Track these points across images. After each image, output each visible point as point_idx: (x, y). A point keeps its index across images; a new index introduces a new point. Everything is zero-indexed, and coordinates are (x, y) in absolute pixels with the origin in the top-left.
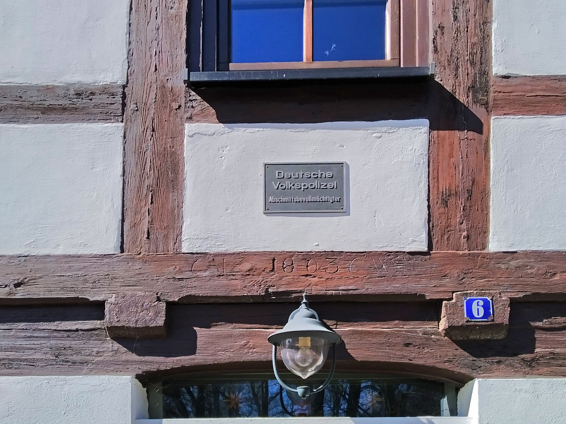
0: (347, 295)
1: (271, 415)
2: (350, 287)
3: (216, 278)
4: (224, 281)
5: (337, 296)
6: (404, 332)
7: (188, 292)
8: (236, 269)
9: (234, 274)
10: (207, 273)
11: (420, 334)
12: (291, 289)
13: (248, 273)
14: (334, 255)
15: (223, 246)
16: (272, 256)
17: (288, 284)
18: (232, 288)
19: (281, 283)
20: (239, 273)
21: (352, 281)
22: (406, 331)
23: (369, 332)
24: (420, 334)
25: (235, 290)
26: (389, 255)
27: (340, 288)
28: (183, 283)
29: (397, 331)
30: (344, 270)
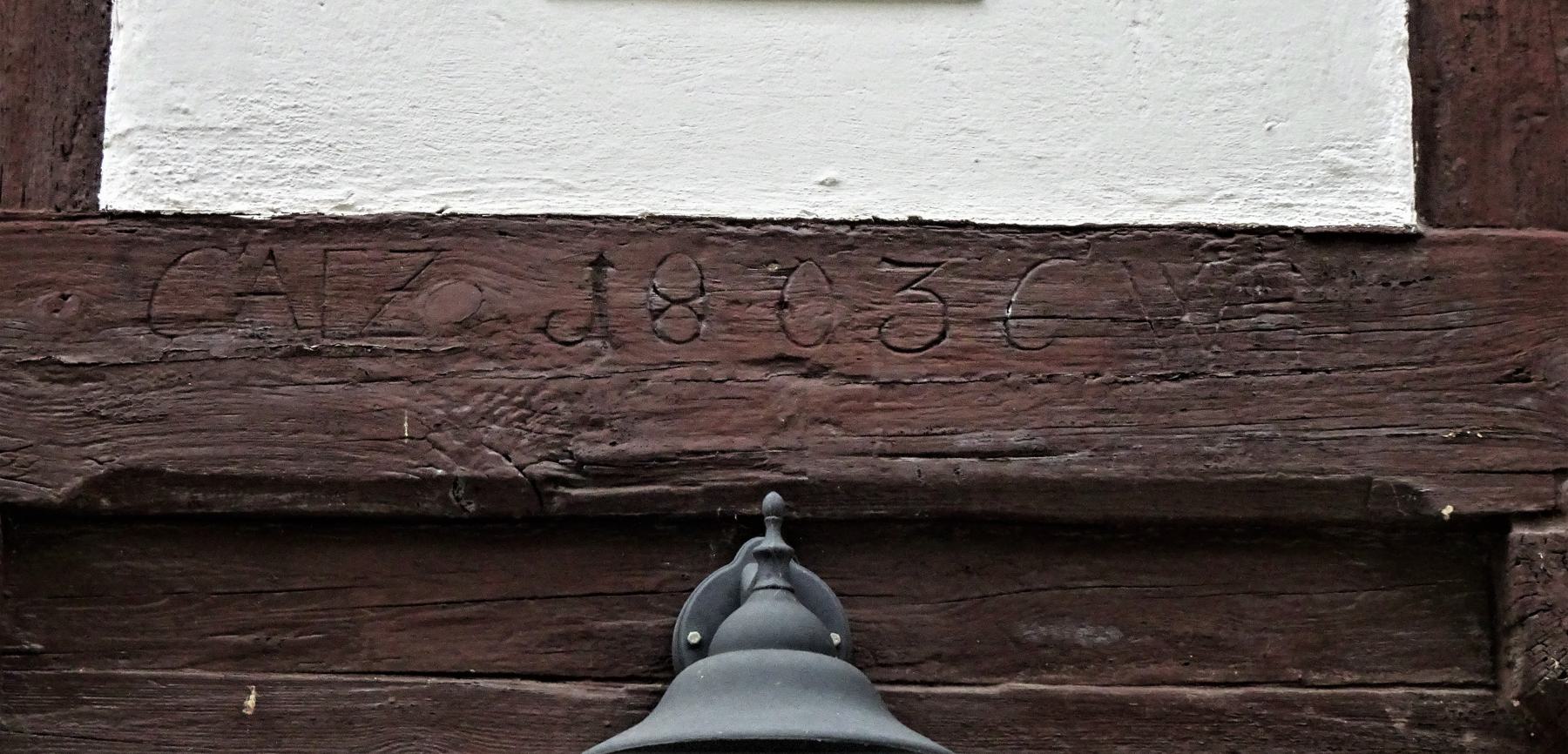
0: (994, 486)
1: (461, 484)
2: (1014, 438)
3: (280, 369)
4: (306, 389)
5: (939, 489)
6: (1310, 713)
7: (124, 450)
8: (392, 316)
9: (380, 344)
10: (222, 342)
11: (1399, 725)
12: (690, 445)
13: (454, 343)
14: (921, 243)
15: (324, 177)
16: (593, 243)
17: (676, 414)
18: (366, 430)
19: (651, 412)
20: (407, 343)
21: (1013, 400)
22: (1324, 706)
23: (1121, 708)
24: (1399, 725)
25: (379, 444)
26: (1215, 249)
27: (962, 442)
28: (97, 394)
29: (1276, 701)
30: (976, 331)
